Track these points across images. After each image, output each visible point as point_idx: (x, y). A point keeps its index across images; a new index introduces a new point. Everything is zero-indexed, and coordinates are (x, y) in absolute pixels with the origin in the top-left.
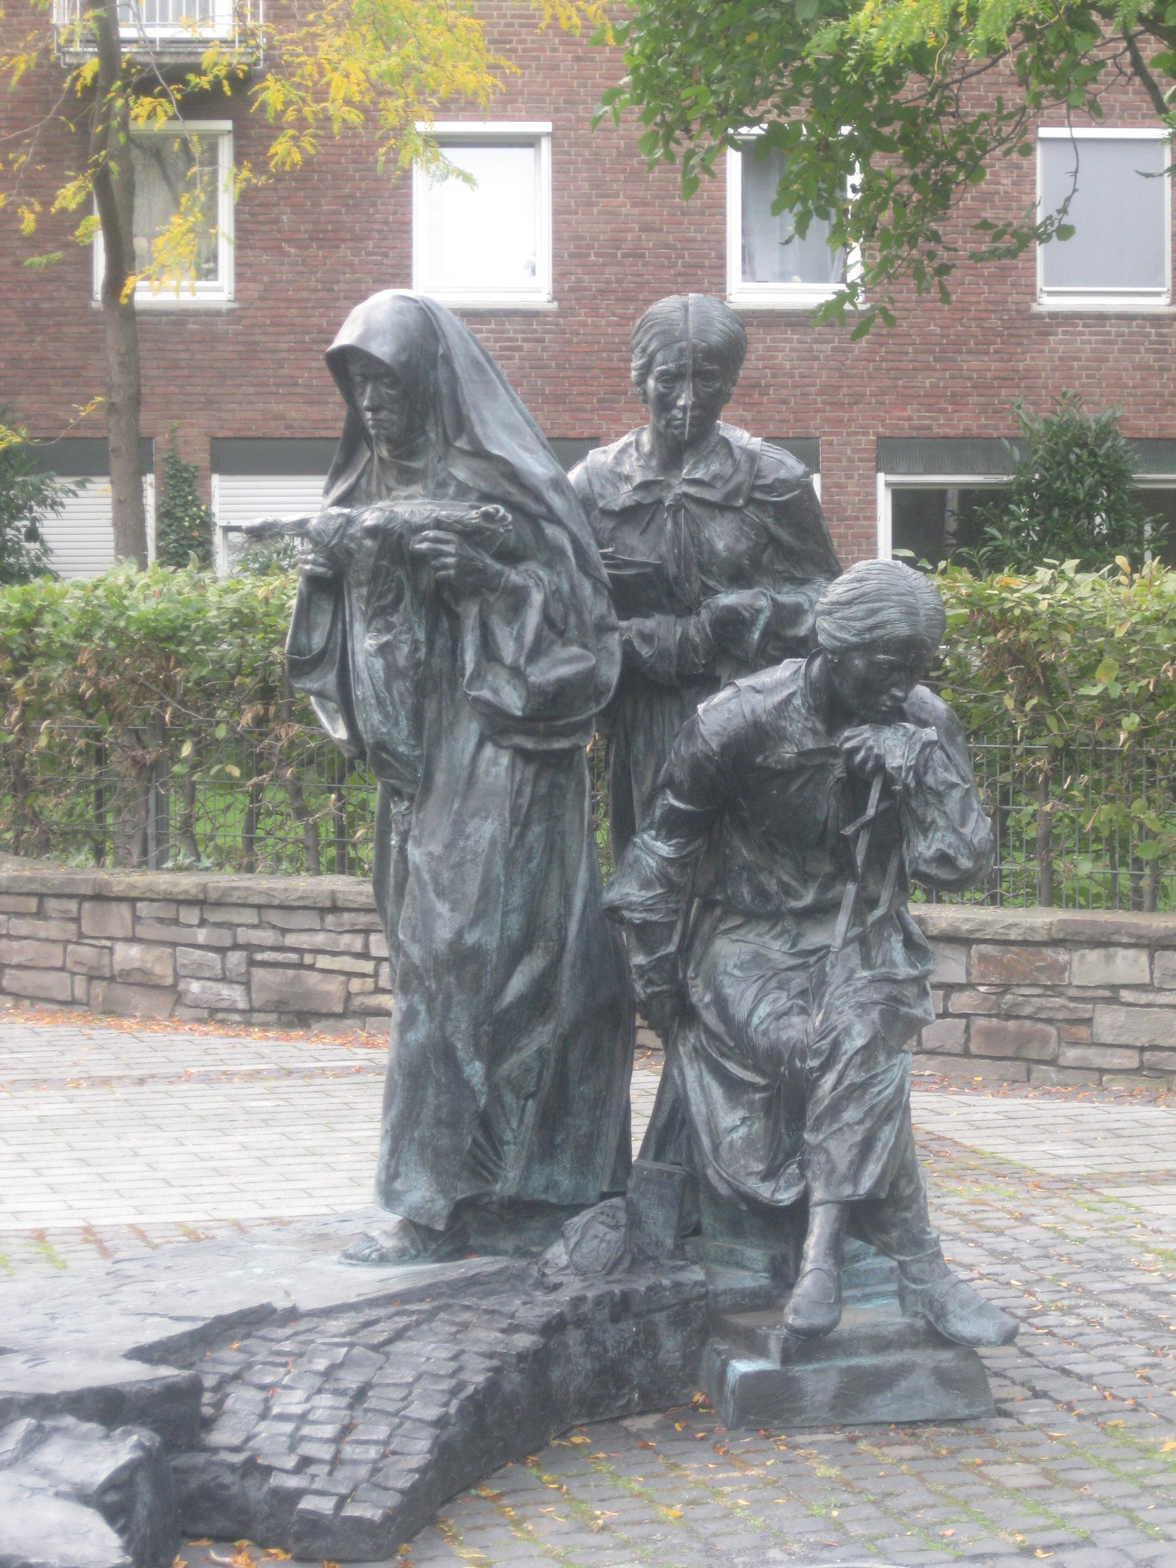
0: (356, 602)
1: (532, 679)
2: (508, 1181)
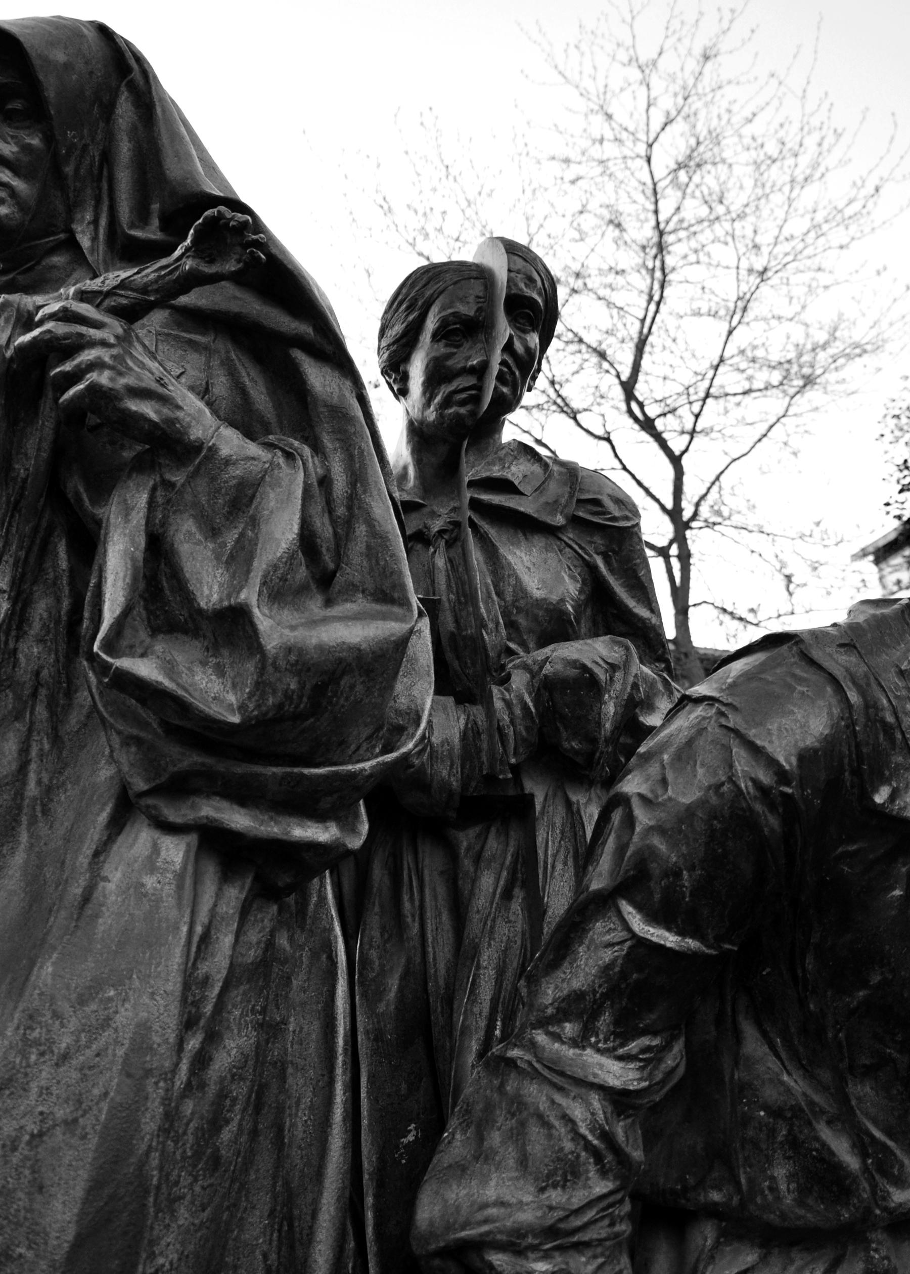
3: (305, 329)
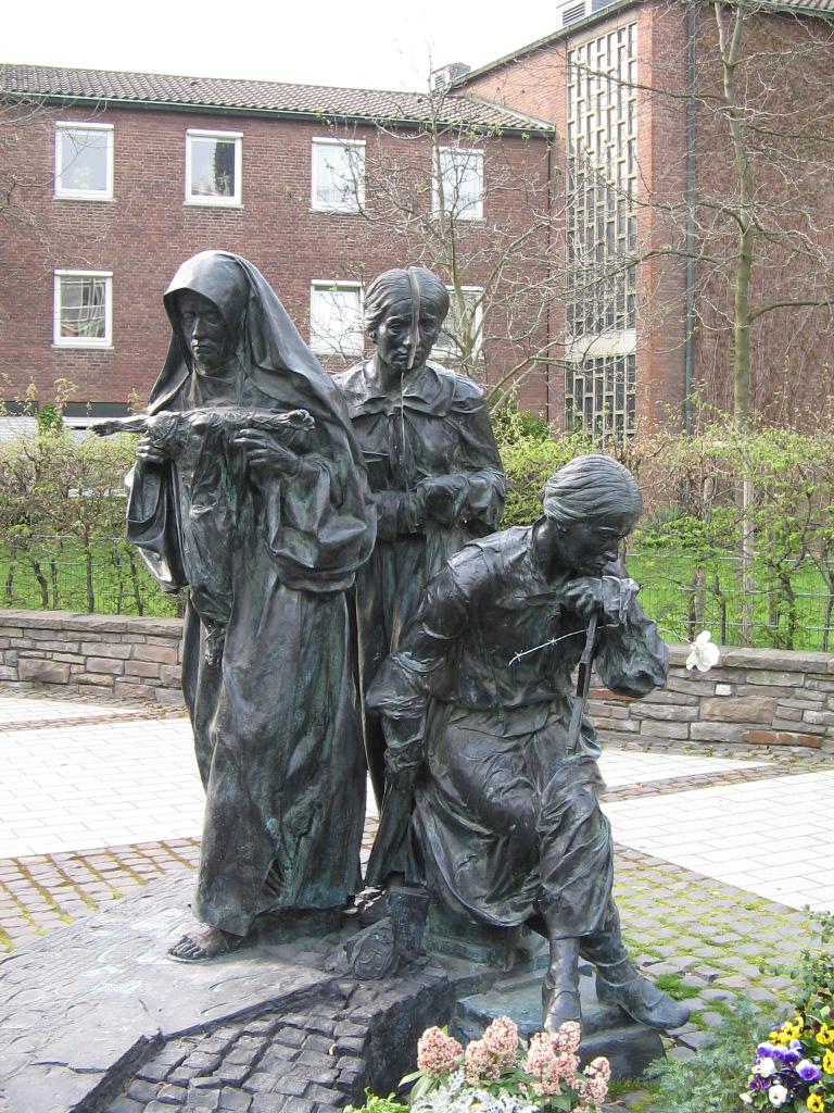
0: (184, 477)
1: (323, 540)
2: (288, 896)
3: (328, 415)
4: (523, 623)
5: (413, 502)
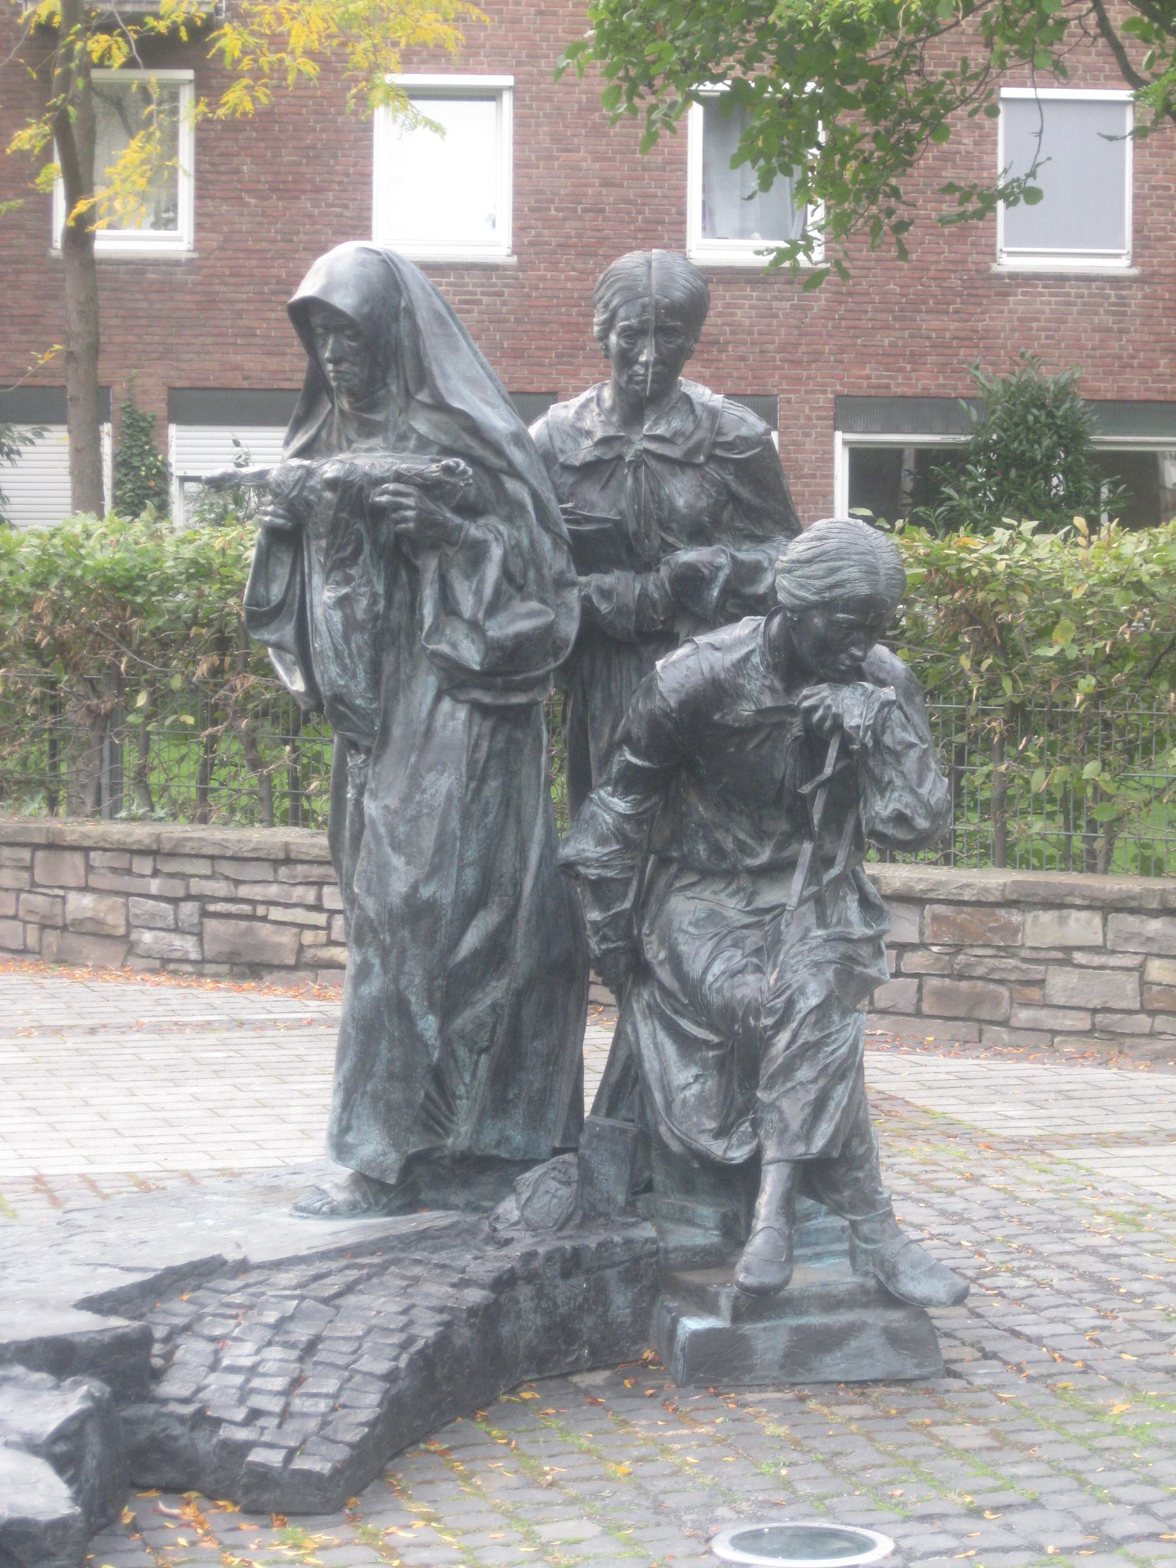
1: (490, 633)
2: (461, 1135)
4: (759, 746)
5: (656, 583)
